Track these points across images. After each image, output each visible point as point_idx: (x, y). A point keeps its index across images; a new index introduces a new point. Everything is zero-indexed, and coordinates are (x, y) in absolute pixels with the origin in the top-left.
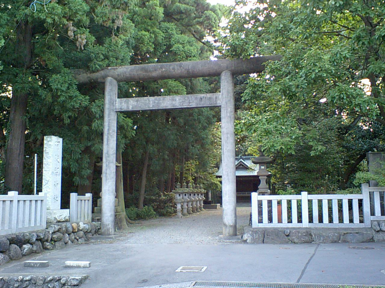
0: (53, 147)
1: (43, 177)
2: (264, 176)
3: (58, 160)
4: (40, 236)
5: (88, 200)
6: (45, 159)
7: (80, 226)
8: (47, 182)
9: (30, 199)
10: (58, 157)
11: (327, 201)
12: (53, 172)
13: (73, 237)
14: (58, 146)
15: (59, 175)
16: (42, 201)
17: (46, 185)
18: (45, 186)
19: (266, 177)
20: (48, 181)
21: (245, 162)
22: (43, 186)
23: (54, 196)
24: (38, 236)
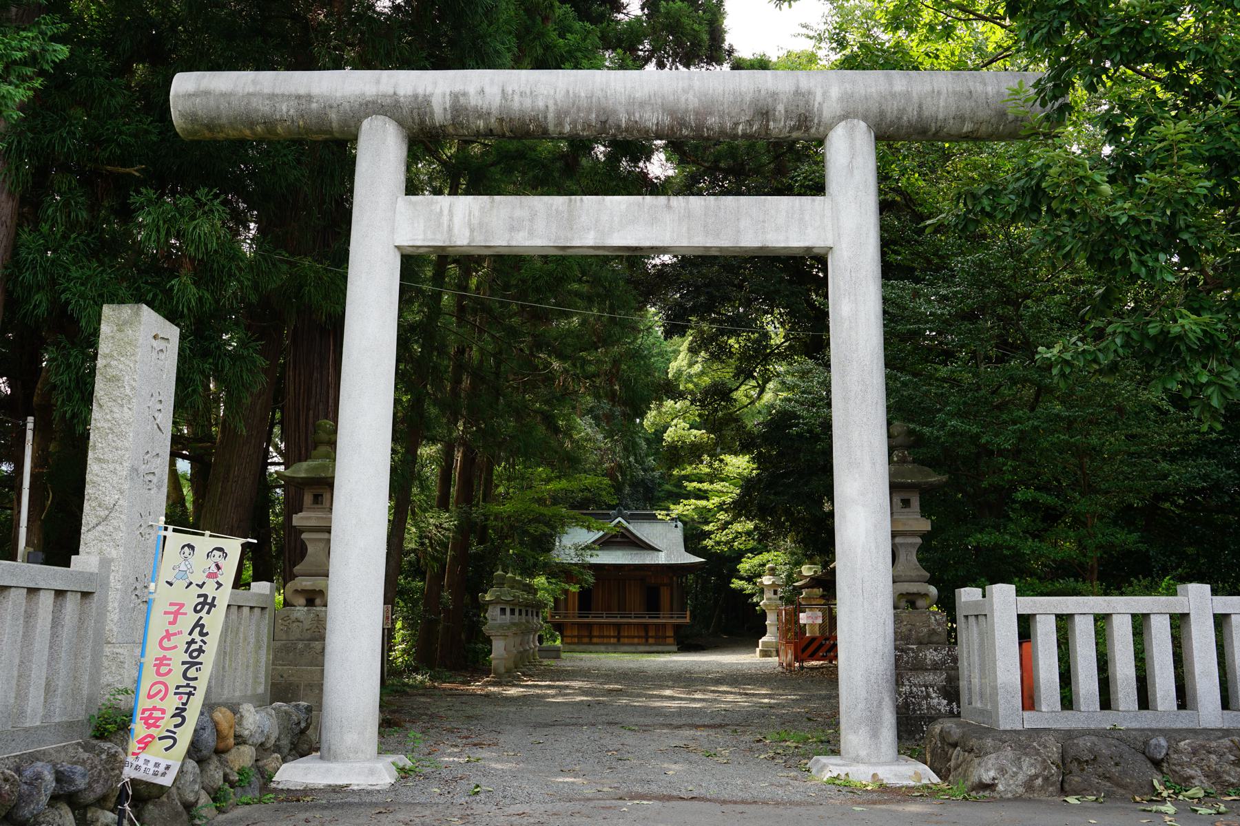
0: (137, 361)
1: (89, 490)
2: (913, 534)
3: (159, 416)
4: (71, 781)
5: (263, 609)
6: (101, 406)
7: (245, 723)
8: (103, 513)
9: (31, 585)
10: (159, 406)
11: (1166, 621)
12: (134, 470)
13: (219, 776)
14: (162, 356)
15: (159, 487)
16: (86, 595)
17: (100, 528)
18: (95, 533)
19: (919, 541)
20: (111, 510)
21: (631, 527)
22: (84, 529)
23: (132, 580)
24: (60, 777)
